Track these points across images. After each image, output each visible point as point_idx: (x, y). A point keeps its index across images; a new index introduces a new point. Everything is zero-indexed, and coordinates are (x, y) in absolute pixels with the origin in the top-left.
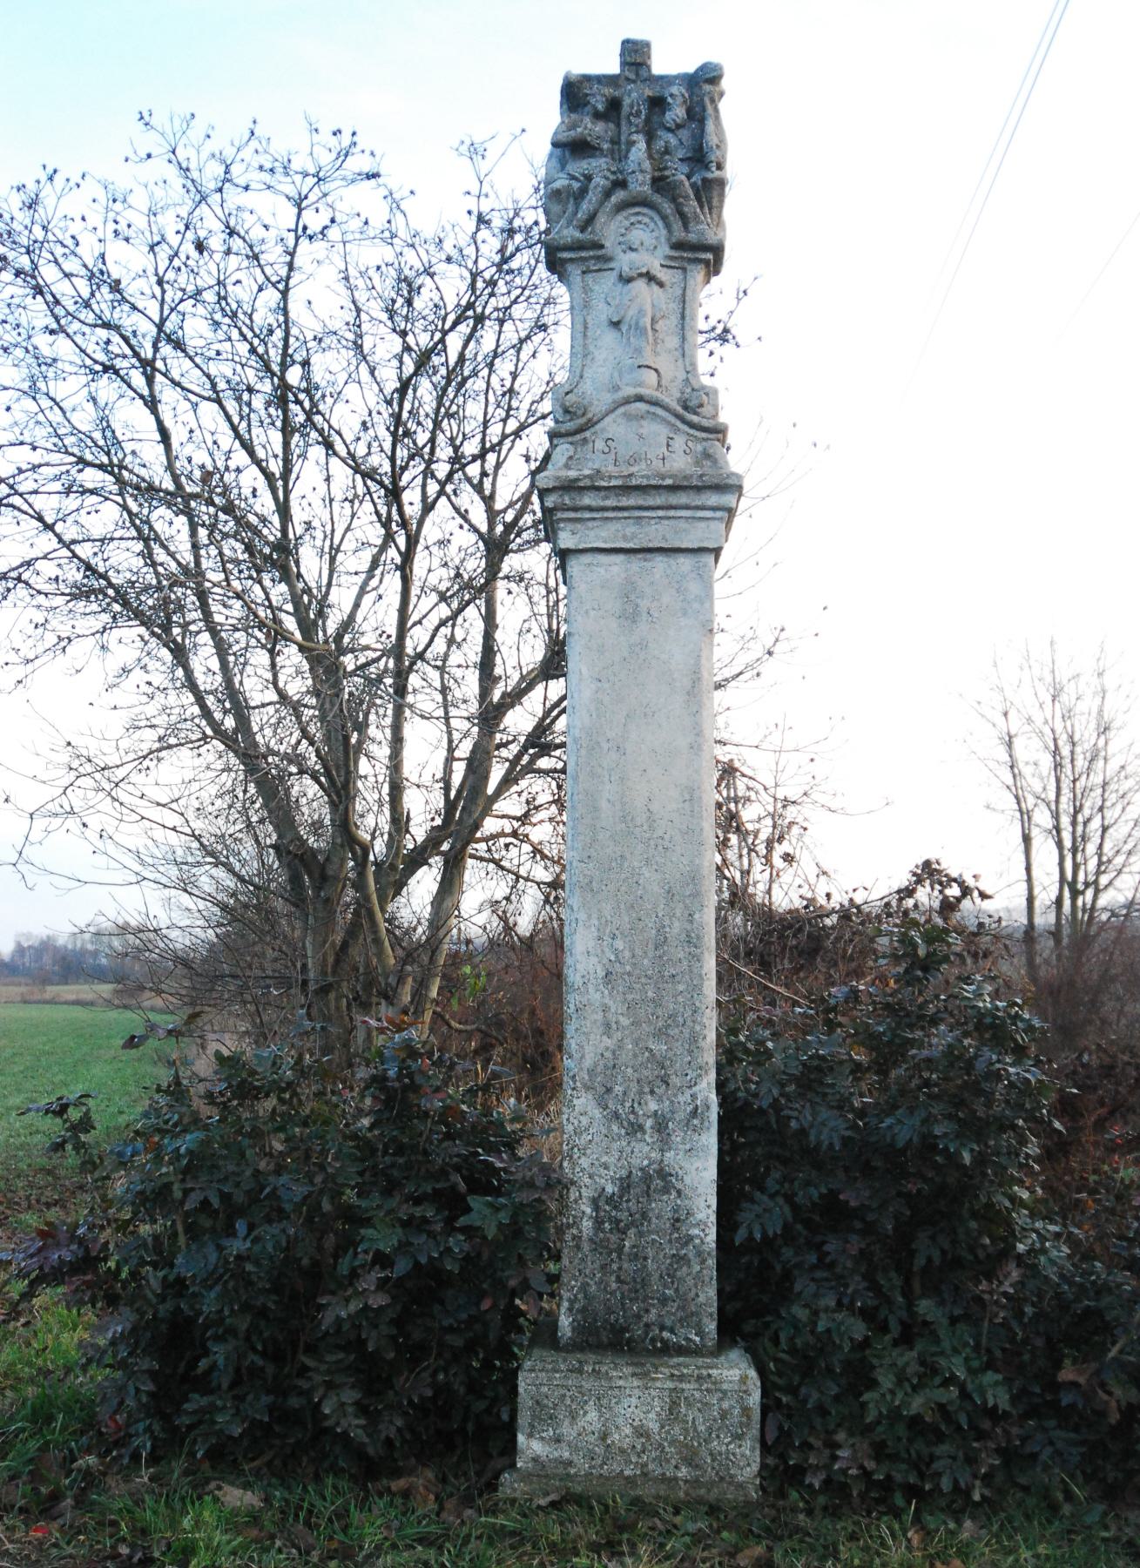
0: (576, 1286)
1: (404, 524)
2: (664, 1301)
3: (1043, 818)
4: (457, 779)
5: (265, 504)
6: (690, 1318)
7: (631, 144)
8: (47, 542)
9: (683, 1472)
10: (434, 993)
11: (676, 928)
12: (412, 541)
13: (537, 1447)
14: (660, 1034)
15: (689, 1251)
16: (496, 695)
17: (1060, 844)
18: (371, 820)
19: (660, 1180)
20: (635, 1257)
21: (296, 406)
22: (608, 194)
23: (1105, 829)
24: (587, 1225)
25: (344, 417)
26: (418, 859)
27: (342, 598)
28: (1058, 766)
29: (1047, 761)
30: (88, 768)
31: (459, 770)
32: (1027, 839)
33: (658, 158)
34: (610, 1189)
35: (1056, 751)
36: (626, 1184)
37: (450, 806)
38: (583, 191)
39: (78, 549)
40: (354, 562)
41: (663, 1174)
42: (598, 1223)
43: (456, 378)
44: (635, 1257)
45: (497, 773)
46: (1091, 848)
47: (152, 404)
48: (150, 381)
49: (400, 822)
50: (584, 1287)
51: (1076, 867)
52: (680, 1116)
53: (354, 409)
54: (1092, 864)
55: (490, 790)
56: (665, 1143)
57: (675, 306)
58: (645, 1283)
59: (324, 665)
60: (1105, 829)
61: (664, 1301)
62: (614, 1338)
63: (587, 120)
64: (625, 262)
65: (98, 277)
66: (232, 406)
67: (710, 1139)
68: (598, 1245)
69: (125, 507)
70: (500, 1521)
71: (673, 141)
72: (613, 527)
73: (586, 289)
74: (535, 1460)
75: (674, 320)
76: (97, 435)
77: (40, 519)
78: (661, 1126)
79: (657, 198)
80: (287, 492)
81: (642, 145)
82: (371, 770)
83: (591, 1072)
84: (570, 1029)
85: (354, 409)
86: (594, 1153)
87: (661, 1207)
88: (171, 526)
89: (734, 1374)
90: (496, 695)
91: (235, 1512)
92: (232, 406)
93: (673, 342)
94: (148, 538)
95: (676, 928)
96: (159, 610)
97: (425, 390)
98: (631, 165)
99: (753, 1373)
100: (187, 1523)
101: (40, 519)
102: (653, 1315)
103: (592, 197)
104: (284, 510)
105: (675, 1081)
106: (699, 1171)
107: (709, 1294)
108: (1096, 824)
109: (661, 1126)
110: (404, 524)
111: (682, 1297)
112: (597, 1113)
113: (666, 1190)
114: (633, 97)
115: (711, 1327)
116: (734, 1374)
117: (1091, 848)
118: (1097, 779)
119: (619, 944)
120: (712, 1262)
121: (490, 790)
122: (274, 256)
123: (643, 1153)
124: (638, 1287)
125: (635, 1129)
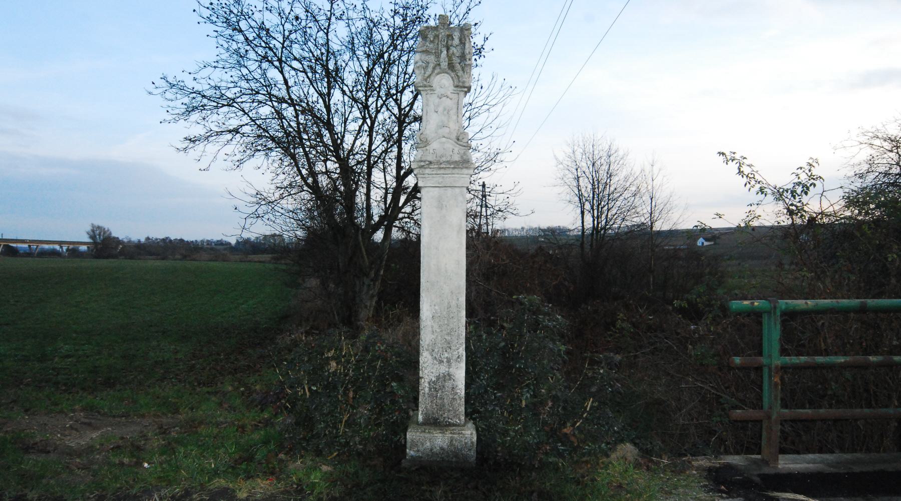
0: (425, 405)
1: (370, 117)
2: (449, 411)
3: (587, 206)
4: (389, 202)
5: (321, 105)
6: (457, 416)
7: (441, 52)
8: (246, 120)
9: (454, 459)
10: (382, 272)
11: (454, 303)
12: (373, 123)
13: (412, 453)
14: (448, 334)
15: (456, 397)
16: (402, 172)
17: (593, 216)
18: (360, 220)
19: (448, 376)
20: (441, 398)
21: (333, 77)
22: (434, 68)
23: (608, 210)
24: (427, 390)
25: (349, 78)
26: (376, 228)
27: (349, 139)
28: (593, 189)
29: (590, 186)
30: (263, 203)
31: (390, 197)
32: (583, 213)
33: (450, 57)
34: (434, 379)
35: (593, 185)
36: (438, 378)
37: (387, 210)
38: (427, 67)
39: (258, 122)
40: (353, 126)
41: (449, 375)
42: (430, 389)
43: (390, 63)
44: (441, 398)
45: (403, 199)
46: (604, 216)
47: (282, 72)
48: (280, 64)
49: (370, 217)
50: (426, 408)
51: (598, 223)
52: (454, 358)
53: (352, 73)
54: (603, 223)
55: (400, 205)
56: (450, 366)
57: (455, 106)
58: (444, 406)
59: (343, 162)
60: (608, 210)
61: (449, 411)
62: (434, 423)
63: (428, 44)
64: (439, 91)
65: (262, 27)
66: (310, 75)
67: (463, 365)
68: (430, 395)
69: (273, 107)
70: (401, 475)
71: (455, 51)
72: (435, 179)
73: (427, 100)
74: (412, 456)
75: (455, 110)
76: (262, 80)
77: (243, 111)
78: (449, 361)
79: (450, 71)
80: (329, 100)
81: (445, 52)
82: (360, 198)
83: (428, 345)
84: (422, 333)
85: (352, 73)
86: (429, 369)
87: (449, 384)
88: (289, 112)
89: (469, 432)
90: (402, 172)
91: (326, 473)
92: (310, 75)
93: (455, 117)
94: (280, 116)
95: (454, 303)
96: (288, 144)
97: (378, 70)
98: (441, 60)
99: (474, 432)
100: (312, 477)
101: (243, 111)
102: (446, 415)
103: (430, 70)
104: (328, 107)
105: (453, 348)
106: (460, 373)
107: (463, 409)
108: (606, 208)
109: (449, 361)
110: (370, 117)
111: (455, 411)
112: (430, 357)
113: (450, 379)
114: (443, 33)
115: (463, 418)
116: (469, 432)
117: (604, 216)
118: (606, 192)
119: (436, 307)
120: (463, 400)
121: (400, 205)
122: (322, 18)
123: (443, 369)
124: (441, 407)
125: (441, 362)
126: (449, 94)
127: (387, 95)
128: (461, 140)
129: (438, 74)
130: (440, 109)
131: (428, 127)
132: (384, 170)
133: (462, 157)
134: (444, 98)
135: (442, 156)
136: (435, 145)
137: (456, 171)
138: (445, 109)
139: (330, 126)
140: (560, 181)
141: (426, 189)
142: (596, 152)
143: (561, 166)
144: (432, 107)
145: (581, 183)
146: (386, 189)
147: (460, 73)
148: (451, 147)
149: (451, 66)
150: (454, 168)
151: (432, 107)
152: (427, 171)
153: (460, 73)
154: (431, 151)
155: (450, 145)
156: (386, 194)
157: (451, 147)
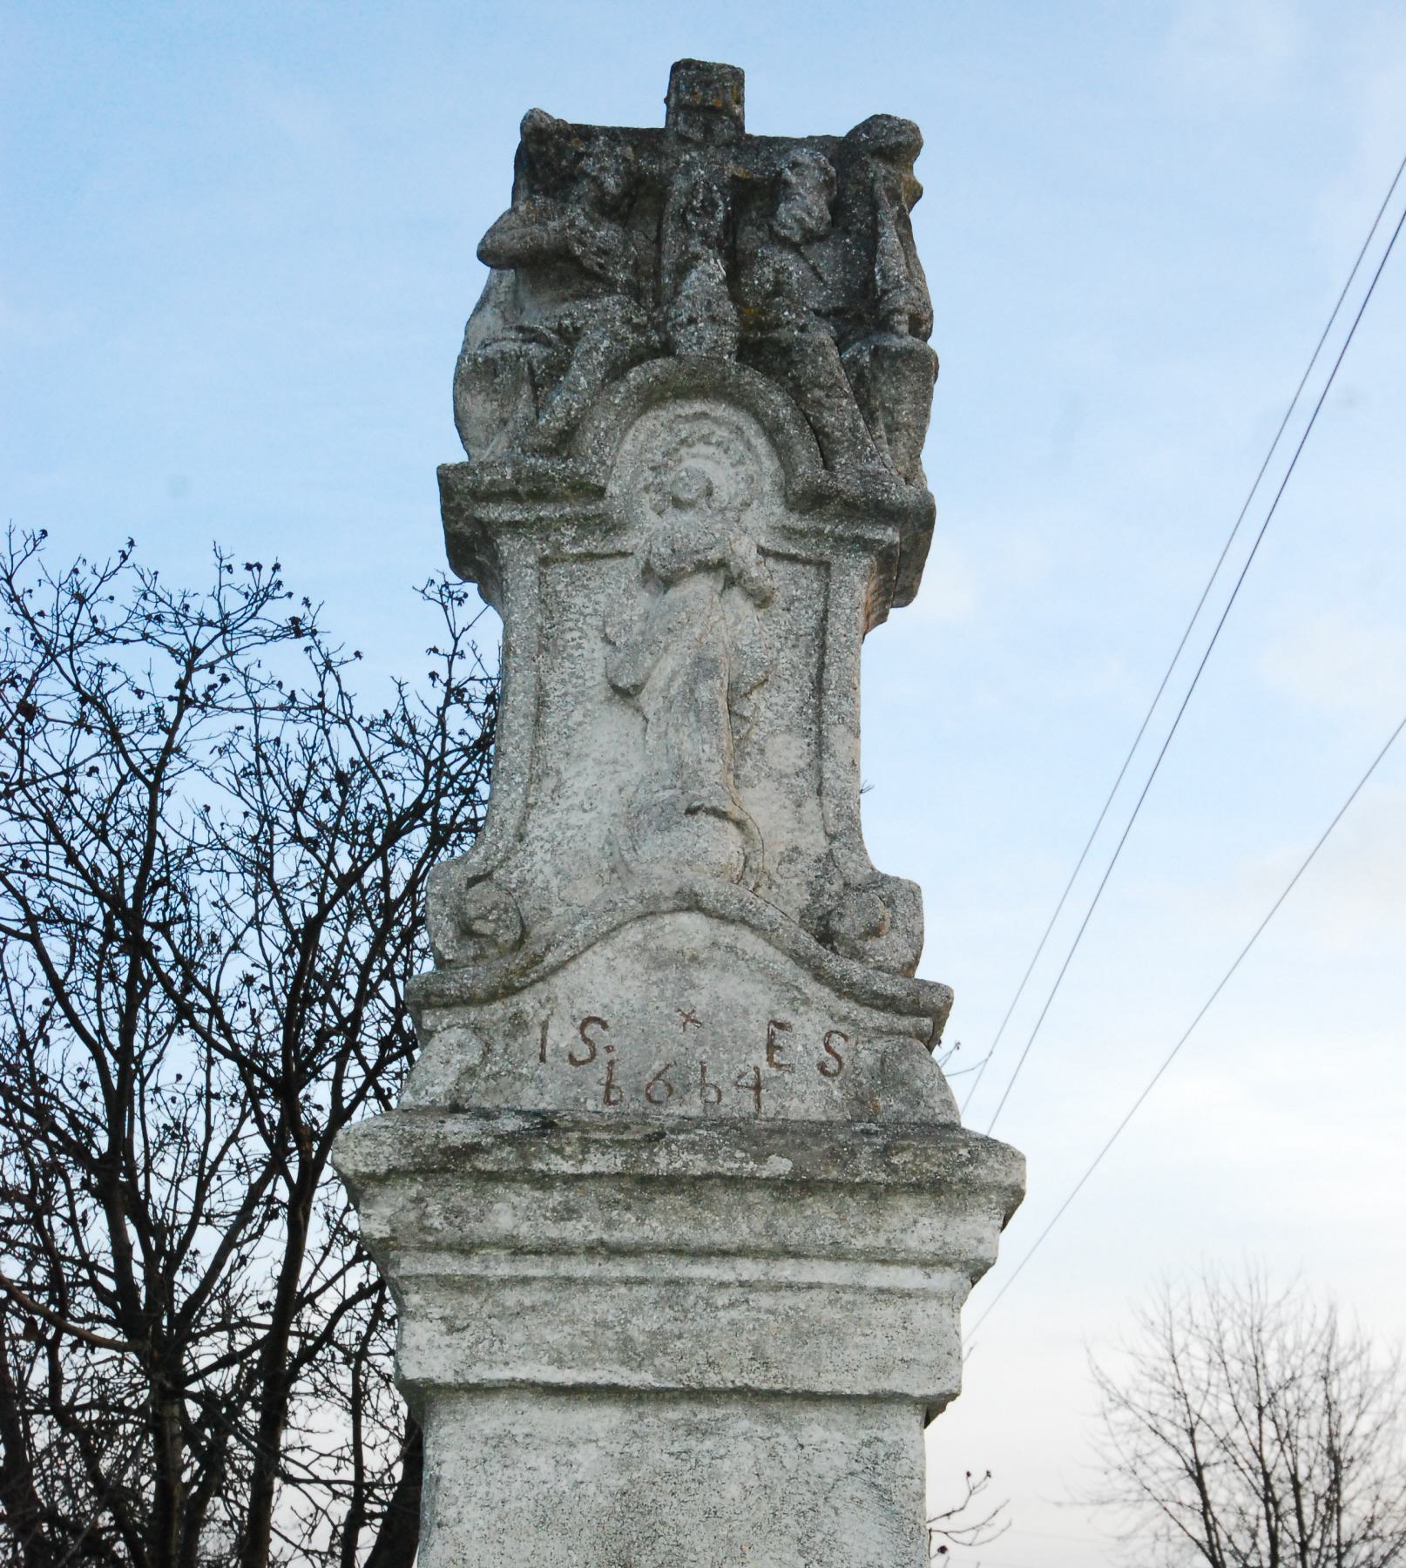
29: (1256, 1508)
35: (1269, 1499)
38: (558, 368)
64: (652, 530)
71: (796, 271)
93: (789, 752)
126: (744, 550)
127: (385, 1043)
128: (855, 939)
129: (651, 398)
130: (665, 671)
131: (541, 826)
132: (356, 1405)
133: (862, 1102)
134: (701, 587)
135: (668, 1083)
136: (602, 982)
137: (820, 1219)
138: (703, 667)
139: (118, 1189)
140: (1121, 1483)
141: (489, 1418)
142: (1271, 1357)
143: (1123, 1415)
144: (590, 660)
145: (1217, 1495)
146: (361, 1489)
147: (841, 414)
148: (763, 1002)
149: (763, 349)
150: (797, 1187)
151: (590, 660)
152: (508, 1214)
153: (841, 414)
154: (563, 1035)
155: (742, 989)
156: (356, 1519)
157: (763, 1002)
